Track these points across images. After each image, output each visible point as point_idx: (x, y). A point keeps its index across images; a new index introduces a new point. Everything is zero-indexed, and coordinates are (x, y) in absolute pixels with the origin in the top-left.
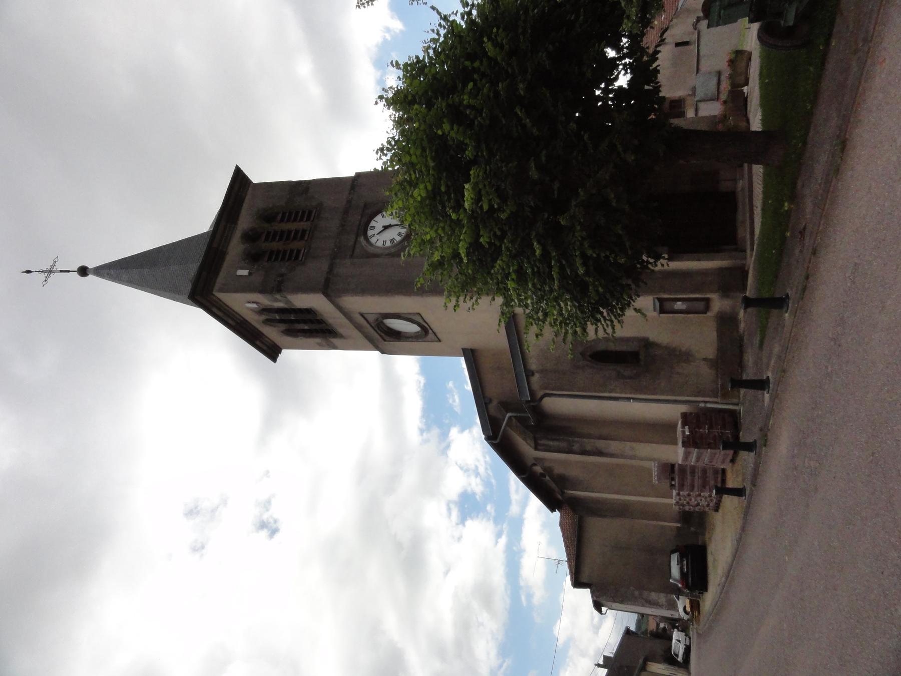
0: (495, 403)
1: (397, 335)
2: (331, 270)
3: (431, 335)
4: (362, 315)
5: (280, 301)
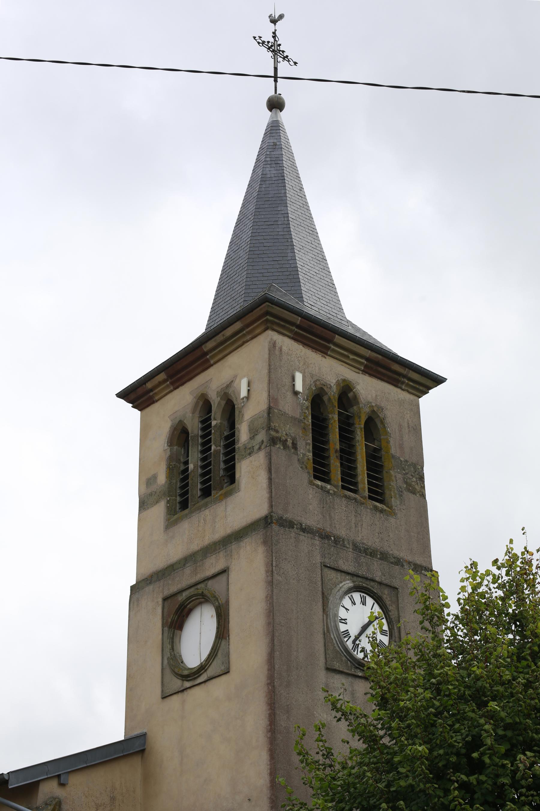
0: (59, 792)
1: (176, 618)
2: (305, 530)
3: (177, 683)
4: (224, 571)
5: (252, 438)
